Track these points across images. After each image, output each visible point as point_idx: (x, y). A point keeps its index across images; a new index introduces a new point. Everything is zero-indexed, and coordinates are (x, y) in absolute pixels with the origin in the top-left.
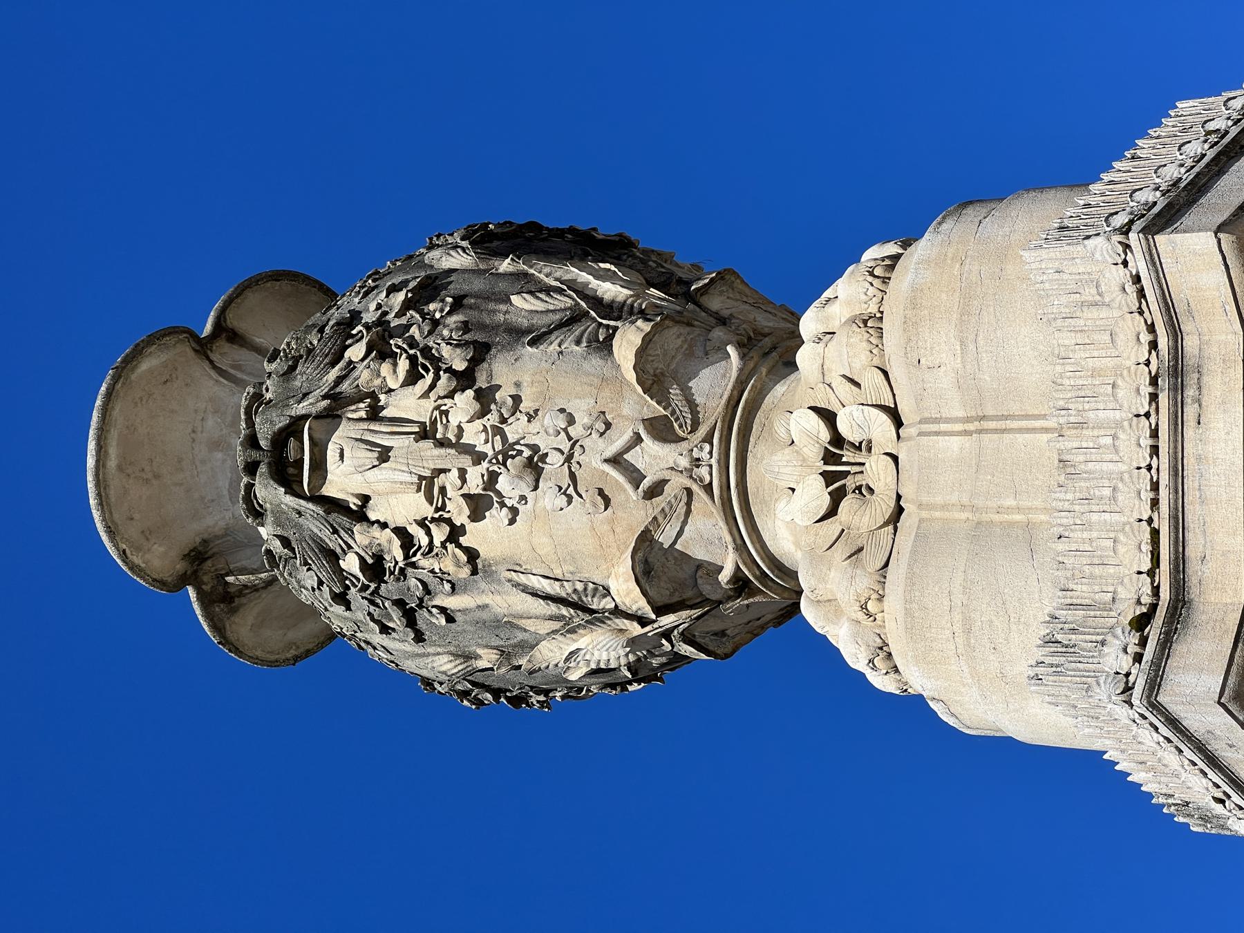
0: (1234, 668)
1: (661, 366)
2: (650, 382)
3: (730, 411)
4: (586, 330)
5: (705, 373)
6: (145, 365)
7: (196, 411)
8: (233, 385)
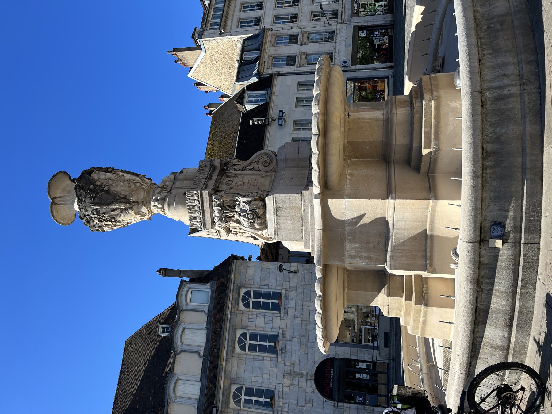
6: (54, 214)
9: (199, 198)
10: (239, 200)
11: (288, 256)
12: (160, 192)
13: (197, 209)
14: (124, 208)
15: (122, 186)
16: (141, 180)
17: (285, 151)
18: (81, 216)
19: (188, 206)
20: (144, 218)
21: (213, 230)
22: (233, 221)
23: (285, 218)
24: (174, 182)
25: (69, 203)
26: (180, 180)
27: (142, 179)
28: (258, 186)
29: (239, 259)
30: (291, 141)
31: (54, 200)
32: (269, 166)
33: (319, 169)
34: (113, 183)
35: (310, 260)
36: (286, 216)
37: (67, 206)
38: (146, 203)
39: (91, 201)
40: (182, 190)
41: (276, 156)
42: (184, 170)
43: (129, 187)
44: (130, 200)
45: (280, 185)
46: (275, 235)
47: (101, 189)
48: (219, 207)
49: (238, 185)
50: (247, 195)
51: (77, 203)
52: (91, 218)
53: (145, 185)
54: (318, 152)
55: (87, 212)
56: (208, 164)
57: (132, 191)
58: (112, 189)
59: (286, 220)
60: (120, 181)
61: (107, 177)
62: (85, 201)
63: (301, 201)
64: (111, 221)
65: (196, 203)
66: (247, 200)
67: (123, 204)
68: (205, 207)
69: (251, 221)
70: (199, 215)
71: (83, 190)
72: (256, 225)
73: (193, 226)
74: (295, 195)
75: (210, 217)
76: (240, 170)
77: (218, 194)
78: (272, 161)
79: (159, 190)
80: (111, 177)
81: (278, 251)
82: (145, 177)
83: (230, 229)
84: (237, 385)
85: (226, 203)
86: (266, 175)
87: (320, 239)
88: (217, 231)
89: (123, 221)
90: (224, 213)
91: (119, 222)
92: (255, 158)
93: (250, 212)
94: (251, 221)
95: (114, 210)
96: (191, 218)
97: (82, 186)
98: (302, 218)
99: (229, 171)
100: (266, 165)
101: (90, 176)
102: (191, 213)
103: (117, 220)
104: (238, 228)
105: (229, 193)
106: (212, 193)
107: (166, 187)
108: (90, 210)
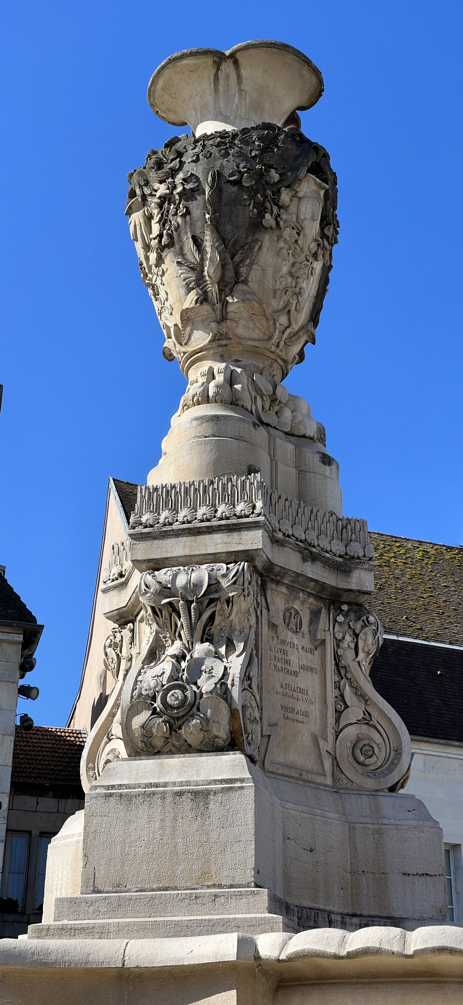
0: (111, 613)
1: (193, 317)
2: (185, 318)
3: (190, 356)
4: (191, 277)
5: (201, 332)
6: (185, 62)
7: (196, 90)
8: (213, 91)
9: (240, 517)
10: (233, 657)
11: (30, 832)
12: (258, 390)
13: (202, 511)
14: (204, 277)
15: (277, 271)
16: (299, 330)
17: (412, 823)
18: (179, 144)
19: (212, 483)
20: (170, 337)
21: (128, 565)
22: (157, 633)
23: (168, 823)
24: (293, 435)
25: (222, 105)
26: (299, 455)
27: (301, 333)
28: (281, 723)
29: (26, 652)
30: (445, 840)
31: (230, 62)
32: (356, 765)
33: (351, 955)
34: (285, 242)
35: (12, 917)
36: (174, 829)
37: (210, 99)
38: (221, 346)
39: (226, 172)
40: (264, 462)
41: (392, 789)
42: (334, 467)
43: (275, 291)
44: (231, 293)
45: (289, 805)
46: (108, 787)
47: (268, 205)
48: (209, 585)
49: (285, 652)
50: (250, 686)
51: (220, 129)
52: (173, 173)
53: (282, 343)
54: (410, 952)
55: (193, 161)
56: (356, 549)
57: (261, 303)
58: (267, 240)
59: (162, 827)
60: (293, 264)
61: (306, 224)
62: (227, 155)
63: (231, 886)
64: (160, 236)
65: (222, 509)
66: (233, 685)
67: (219, 274)
68: (207, 537)
69: (159, 699)
70: (180, 517)
71: (264, 151)
72: (145, 715)
73: (142, 497)
74: (251, 862)
75: (174, 555)
76: (337, 658)
77: (254, 583)
78: (375, 773)
79: (267, 388)
80: (305, 236)
81: (51, 794)
82: (306, 342)
83: (130, 625)
84: (291, 618)
85: (222, 609)
86: (325, 755)
87: (91, 958)
88: (123, 579)
89: (160, 273)
90: (188, 603)
91: (160, 261)
92: (382, 712)
93: (188, 694)
94: (159, 699)
95: (198, 242)
96: (169, 490)
97: (277, 146)
98: (166, 889)
99: (335, 621)
100: (358, 751)
101: (310, 171)
102: (187, 491)
103: (164, 254)
104: (134, 652)
105: (257, 622)
106: (257, 563)
107: (276, 408)
108: (198, 170)
